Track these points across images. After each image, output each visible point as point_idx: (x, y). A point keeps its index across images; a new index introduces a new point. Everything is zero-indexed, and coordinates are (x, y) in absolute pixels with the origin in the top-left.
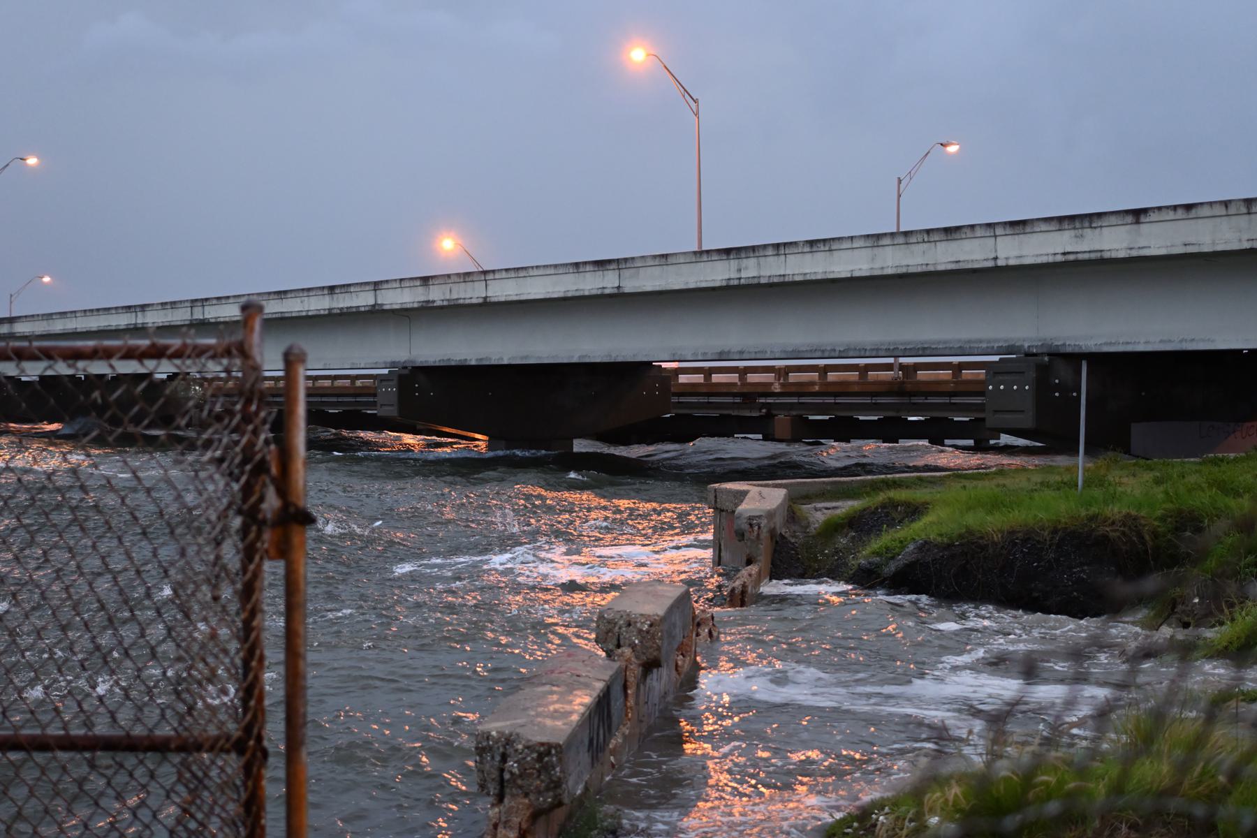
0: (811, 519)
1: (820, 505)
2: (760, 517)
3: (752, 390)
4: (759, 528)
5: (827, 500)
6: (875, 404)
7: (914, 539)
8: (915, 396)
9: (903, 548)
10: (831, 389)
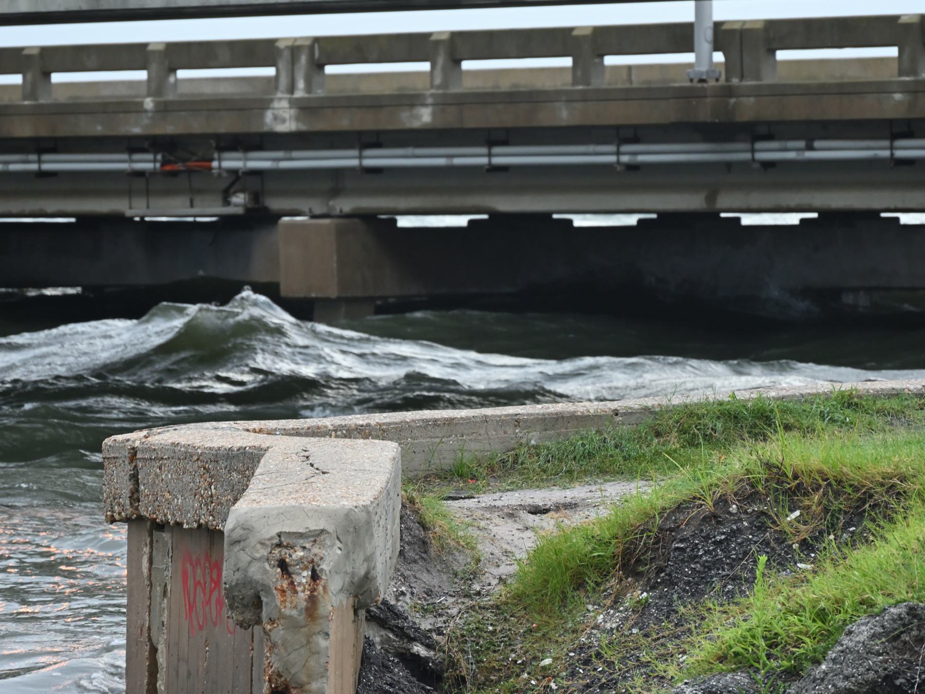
0: (485, 549)
1: (513, 498)
2: (317, 536)
3: (197, 125)
4: (315, 577)
5: (529, 480)
6: (632, 168)
7: (868, 603)
8: (769, 137)
9: (828, 637)
10: (474, 119)
